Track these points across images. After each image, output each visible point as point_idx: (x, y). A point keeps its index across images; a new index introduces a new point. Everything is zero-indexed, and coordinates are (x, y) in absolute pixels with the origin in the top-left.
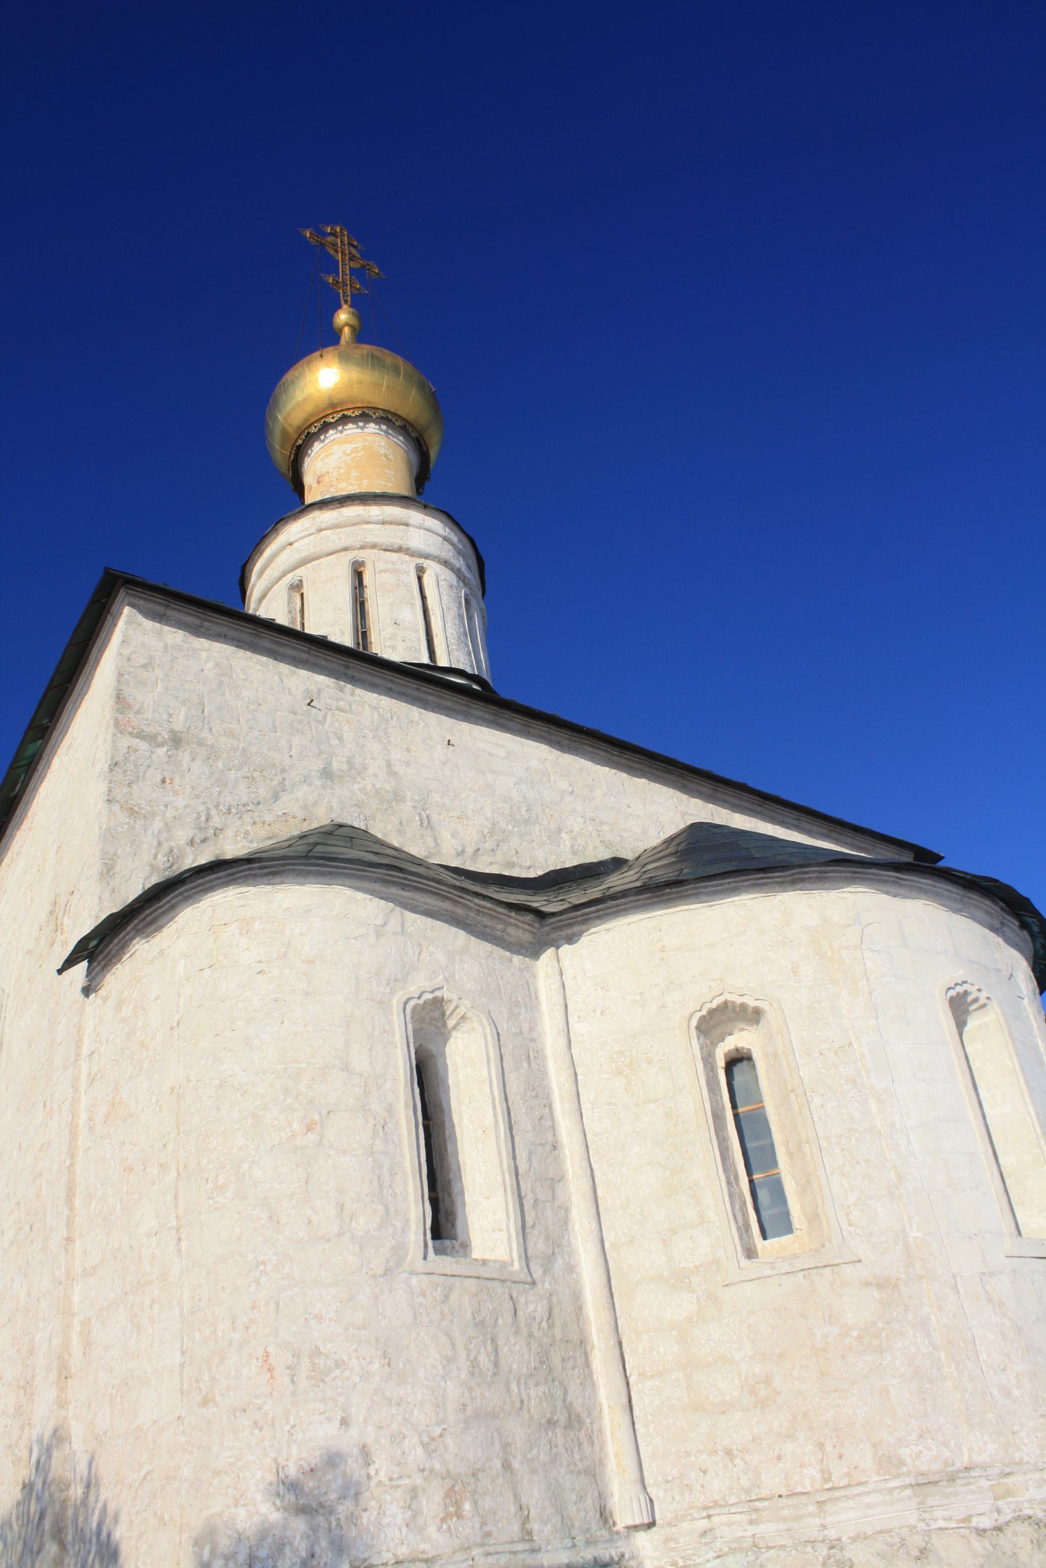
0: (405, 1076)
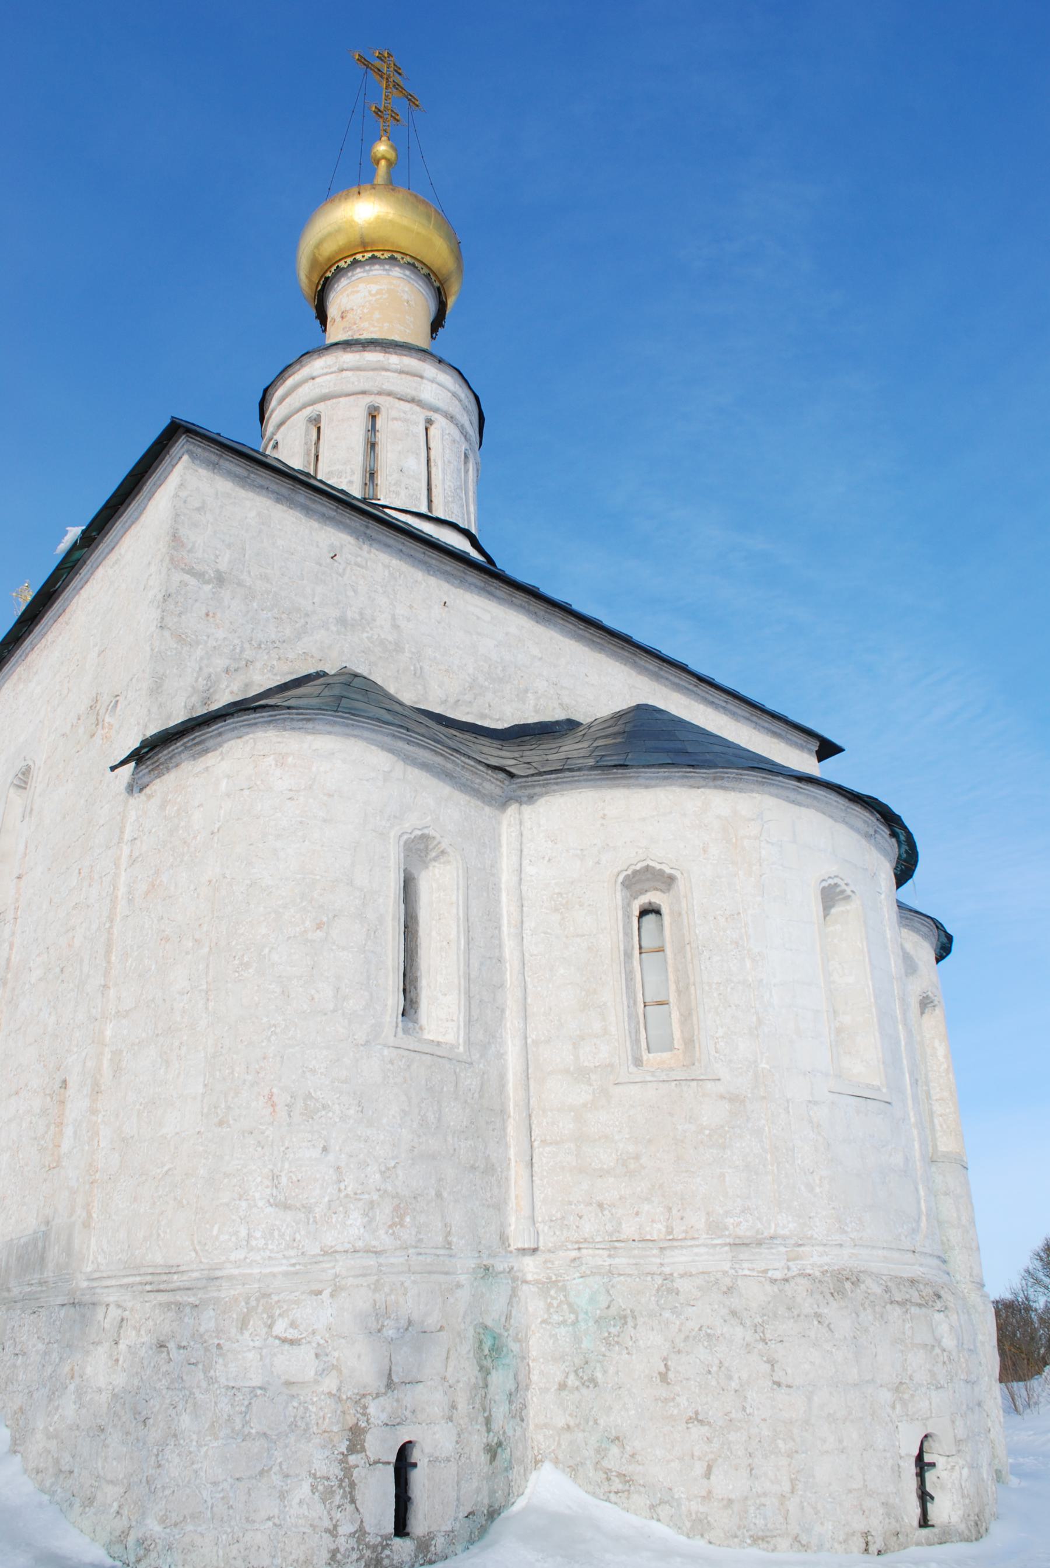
0: (395, 894)
